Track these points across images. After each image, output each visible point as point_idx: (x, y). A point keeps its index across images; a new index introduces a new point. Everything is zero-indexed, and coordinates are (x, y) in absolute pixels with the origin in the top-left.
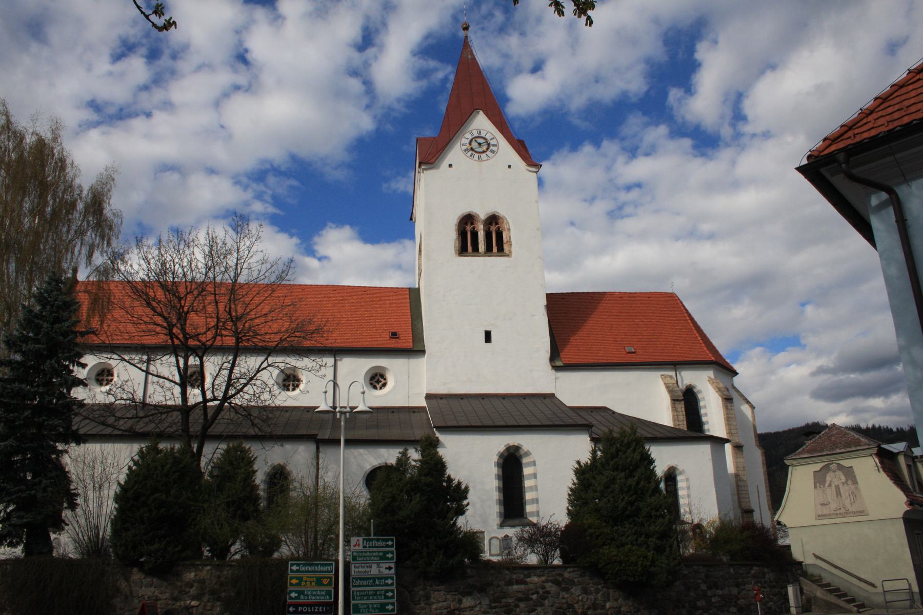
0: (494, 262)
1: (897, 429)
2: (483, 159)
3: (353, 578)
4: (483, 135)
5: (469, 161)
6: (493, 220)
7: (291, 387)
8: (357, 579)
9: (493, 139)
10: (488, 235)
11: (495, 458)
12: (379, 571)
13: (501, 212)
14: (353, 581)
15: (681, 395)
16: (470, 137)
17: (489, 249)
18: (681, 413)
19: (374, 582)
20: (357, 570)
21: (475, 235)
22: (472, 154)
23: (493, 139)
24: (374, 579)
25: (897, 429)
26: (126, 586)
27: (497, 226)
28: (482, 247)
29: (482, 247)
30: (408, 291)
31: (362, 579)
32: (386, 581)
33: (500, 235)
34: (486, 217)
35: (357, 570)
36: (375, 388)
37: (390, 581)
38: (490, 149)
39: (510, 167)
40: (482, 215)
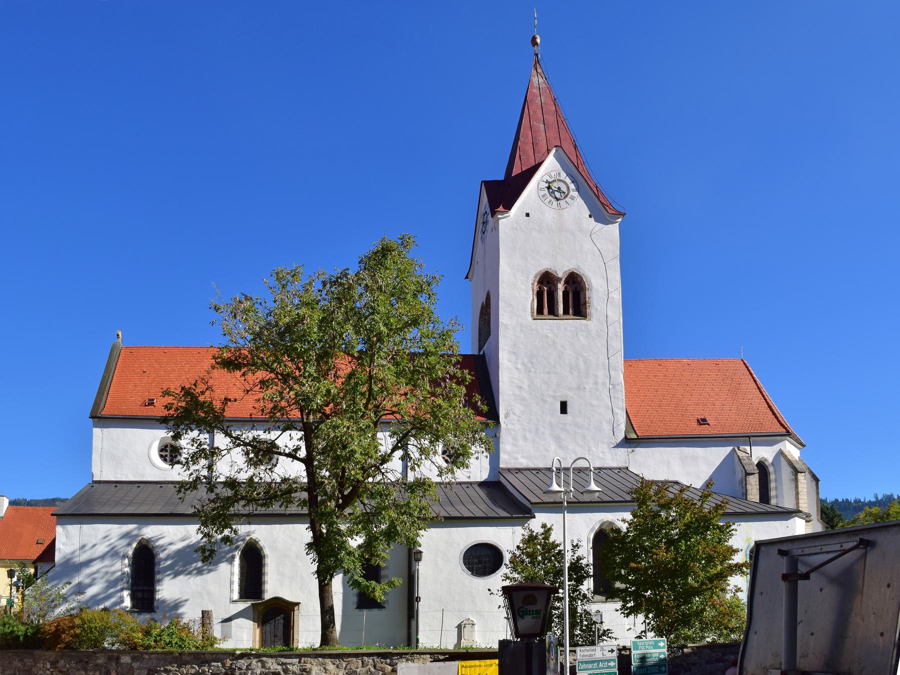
0: (572, 324)
1: (843, 500)
3: (579, 662)
7: (164, 454)
8: (582, 663)
12: (603, 654)
14: (579, 665)
15: (472, 460)
17: (566, 312)
18: (755, 486)
19: (598, 665)
20: (582, 654)
24: (598, 661)
25: (843, 500)
26: (161, 656)
27: (575, 285)
31: (586, 662)
32: (609, 664)
35: (582, 654)
36: (161, 450)
37: (612, 664)
38: (569, 196)
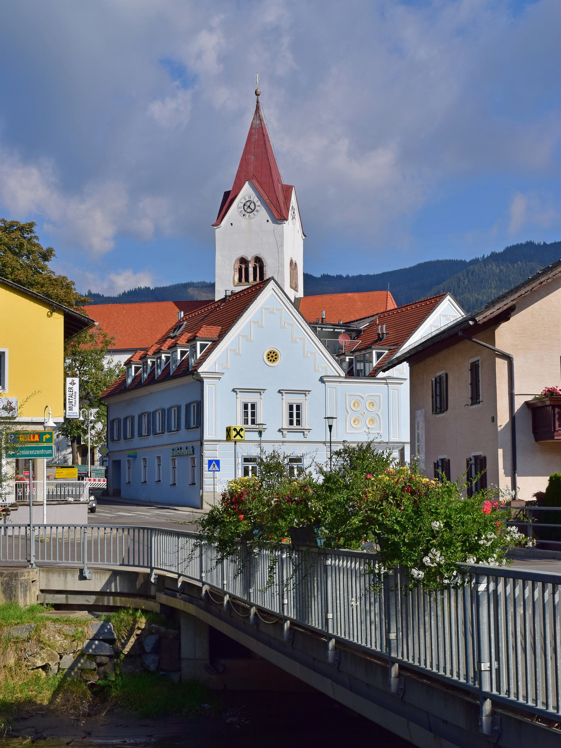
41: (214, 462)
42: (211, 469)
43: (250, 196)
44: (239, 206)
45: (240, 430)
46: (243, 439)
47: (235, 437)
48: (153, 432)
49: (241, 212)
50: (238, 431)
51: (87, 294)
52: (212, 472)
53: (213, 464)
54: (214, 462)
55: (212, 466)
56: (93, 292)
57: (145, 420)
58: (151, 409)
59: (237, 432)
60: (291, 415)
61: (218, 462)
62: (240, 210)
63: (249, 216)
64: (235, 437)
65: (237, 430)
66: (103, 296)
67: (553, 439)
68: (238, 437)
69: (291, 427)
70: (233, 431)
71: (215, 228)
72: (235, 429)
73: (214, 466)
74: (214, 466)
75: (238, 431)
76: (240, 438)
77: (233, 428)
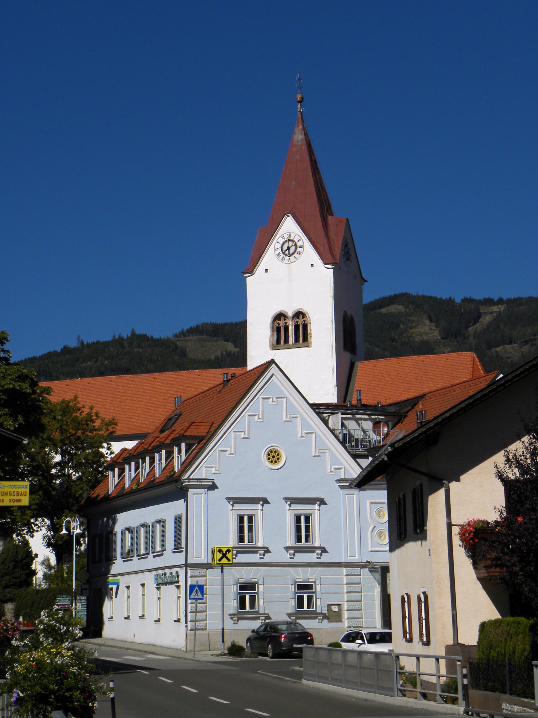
2: (292, 261)
4: (296, 255)
5: (280, 263)
6: (299, 314)
9: (299, 240)
10: (297, 328)
11: (479, 624)
13: (305, 309)
16: (281, 241)
17: (297, 340)
21: (286, 329)
22: (283, 257)
23: (299, 240)
28: (292, 339)
29: (292, 339)
30: (448, 702)
33: (305, 327)
34: (293, 314)
39: (312, 265)
40: (290, 314)
41: (197, 588)
42: (192, 596)
43: (290, 234)
44: (276, 247)
45: (226, 551)
46: (231, 562)
47: (220, 560)
48: (137, 552)
49: (278, 254)
50: (224, 552)
51: (129, 335)
52: (362, 561)
53: (195, 590)
54: (197, 588)
55: (194, 593)
56: (138, 332)
57: (128, 536)
58: (134, 524)
59: (223, 554)
60: (298, 529)
61: (201, 588)
62: (277, 252)
63: (289, 260)
64: (220, 560)
65: (222, 551)
66: (152, 337)
67: (265, 617)
68: (224, 561)
69: (299, 544)
70: (218, 553)
71: (245, 275)
72: (220, 551)
73: (197, 593)
74: (197, 593)
75: (224, 552)
76: (226, 561)
77: (218, 549)
